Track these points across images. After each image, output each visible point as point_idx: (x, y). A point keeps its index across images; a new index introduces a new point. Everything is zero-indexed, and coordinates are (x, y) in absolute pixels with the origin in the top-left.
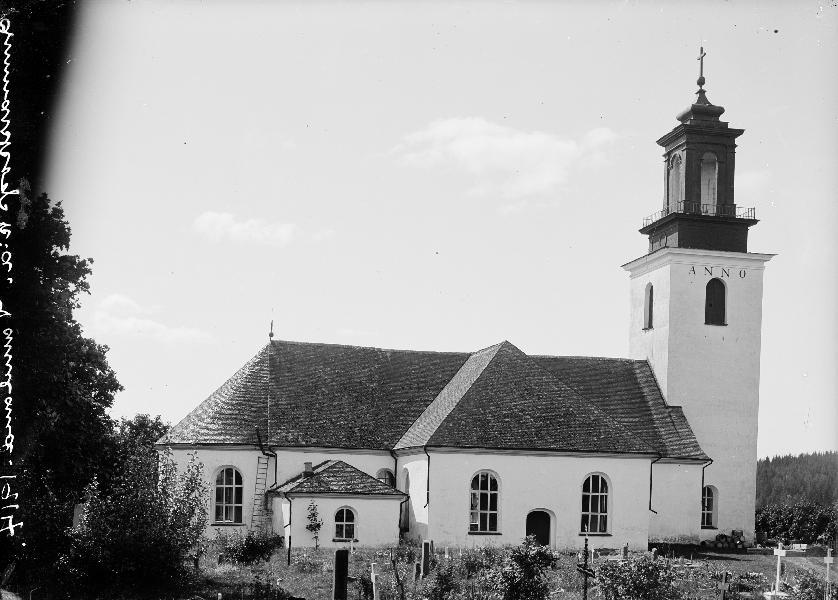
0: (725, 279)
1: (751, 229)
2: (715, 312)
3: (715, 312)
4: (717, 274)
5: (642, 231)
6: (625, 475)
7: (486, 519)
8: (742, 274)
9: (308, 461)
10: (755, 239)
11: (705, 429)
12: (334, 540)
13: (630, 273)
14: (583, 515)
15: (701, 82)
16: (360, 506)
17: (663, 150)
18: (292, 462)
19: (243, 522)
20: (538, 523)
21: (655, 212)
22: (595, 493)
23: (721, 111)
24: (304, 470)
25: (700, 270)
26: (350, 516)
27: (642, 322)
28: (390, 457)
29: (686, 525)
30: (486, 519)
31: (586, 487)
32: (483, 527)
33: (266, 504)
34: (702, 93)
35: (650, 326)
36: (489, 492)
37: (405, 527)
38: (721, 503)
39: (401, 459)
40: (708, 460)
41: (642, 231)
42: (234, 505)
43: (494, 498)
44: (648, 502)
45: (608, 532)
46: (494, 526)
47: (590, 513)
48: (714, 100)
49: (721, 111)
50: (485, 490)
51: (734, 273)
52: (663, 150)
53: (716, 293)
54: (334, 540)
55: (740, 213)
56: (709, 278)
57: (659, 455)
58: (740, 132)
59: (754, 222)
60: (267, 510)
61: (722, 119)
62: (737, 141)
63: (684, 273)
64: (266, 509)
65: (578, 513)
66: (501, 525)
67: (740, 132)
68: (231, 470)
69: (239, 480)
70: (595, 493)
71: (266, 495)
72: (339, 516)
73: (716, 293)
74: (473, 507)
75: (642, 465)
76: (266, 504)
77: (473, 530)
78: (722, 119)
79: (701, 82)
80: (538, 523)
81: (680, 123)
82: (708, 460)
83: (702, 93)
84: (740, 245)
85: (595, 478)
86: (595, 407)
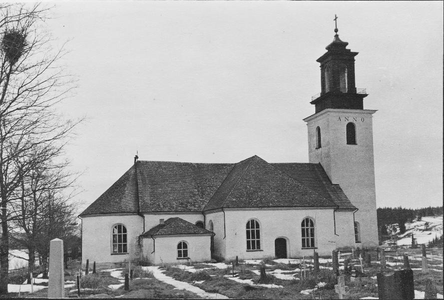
2: (351, 139)
3: (351, 139)
4: (351, 120)
5: (312, 103)
6: (322, 217)
7: (254, 243)
8: (363, 120)
9: (162, 218)
10: (367, 104)
11: (352, 195)
12: (177, 259)
13: (307, 123)
14: (247, 241)
15: (336, 31)
16: (190, 240)
17: (319, 64)
18: (153, 220)
19: (128, 252)
20: (281, 246)
22: (308, 227)
23: (347, 44)
25: (343, 119)
26: (185, 246)
29: (348, 240)
30: (254, 243)
33: (139, 243)
34: (337, 36)
36: (255, 229)
37: (413, 242)
38: (361, 229)
41: (312, 103)
43: (258, 232)
44: (333, 231)
45: (261, 249)
46: (259, 247)
48: (343, 38)
49: (347, 44)
50: (253, 231)
51: (359, 119)
52: (319, 64)
53: (351, 128)
54: (177, 259)
55: (358, 92)
56: (347, 122)
57: (337, 209)
58: (356, 54)
59: (366, 95)
60: (140, 245)
61: (347, 48)
62: (356, 58)
63: (336, 120)
67: (356, 54)
68: (254, 220)
70: (308, 227)
71: (139, 237)
72: (179, 246)
73: (351, 128)
74: (114, 241)
75: (329, 212)
76: (139, 243)
77: (114, 253)
78: (347, 48)
79: (336, 31)
80: (281, 246)
81: (327, 51)
82: (356, 209)
83: (337, 36)
84: (360, 106)
85: (253, 221)
86: (310, 185)
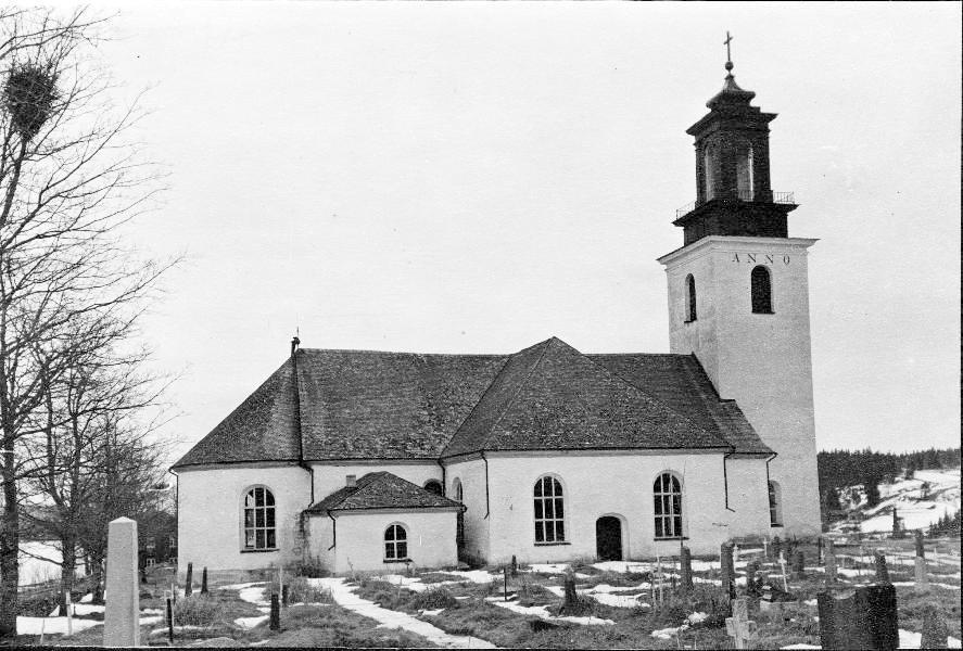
0: (769, 265)
1: (791, 215)
2: (762, 301)
3: (762, 301)
4: (761, 261)
5: (677, 223)
6: (698, 471)
7: (550, 527)
8: (787, 260)
9: (352, 474)
11: (762, 422)
12: (385, 562)
13: (665, 267)
15: (729, 67)
16: (411, 521)
17: (693, 139)
18: (331, 478)
19: (277, 547)
20: (609, 534)
21: (688, 202)
22: (667, 492)
23: (752, 95)
24: (345, 485)
25: (743, 258)
26: (402, 533)
27: (684, 311)
28: (439, 468)
30: (550, 527)
31: (537, 492)
32: (260, 544)
33: (302, 526)
34: (730, 78)
35: (693, 317)
36: (554, 498)
37: (896, 526)
39: (449, 468)
40: (771, 453)
41: (677, 223)
42: (266, 528)
43: (560, 504)
44: (722, 501)
45: (566, 540)
46: (561, 536)
47: (663, 516)
48: (744, 84)
49: (752, 95)
51: (779, 259)
52: (693, 139)
53: (761, 277)
54: (385, 562)
55: (777, 199)
56: (753, 265)
57: (731, 453)
58: (772, 116)
59: (794, 207)
61: (753, 103)
63: (729, 260)
64: (302, 530)
65: (531, 520)
66: (569, 534)
67: (772, 116)
69: (271, 500)
70: (667, 492)
72: (389, 535)
73: (761, 277)
75: (716, 459)
76: (302, 526)
77: (248, 550)
78: (753, 103)
80: (609, 534)
81: (710, 110)
83: (730, 78)
84: (780, 230)
85: (548, 480)
86: (675, 401)
